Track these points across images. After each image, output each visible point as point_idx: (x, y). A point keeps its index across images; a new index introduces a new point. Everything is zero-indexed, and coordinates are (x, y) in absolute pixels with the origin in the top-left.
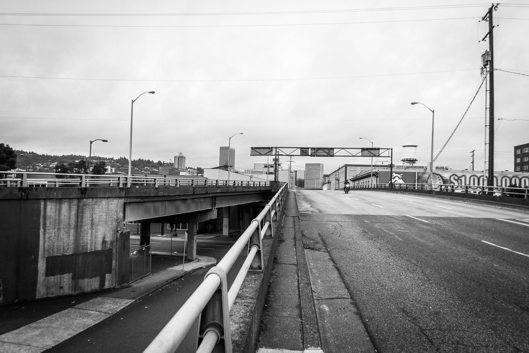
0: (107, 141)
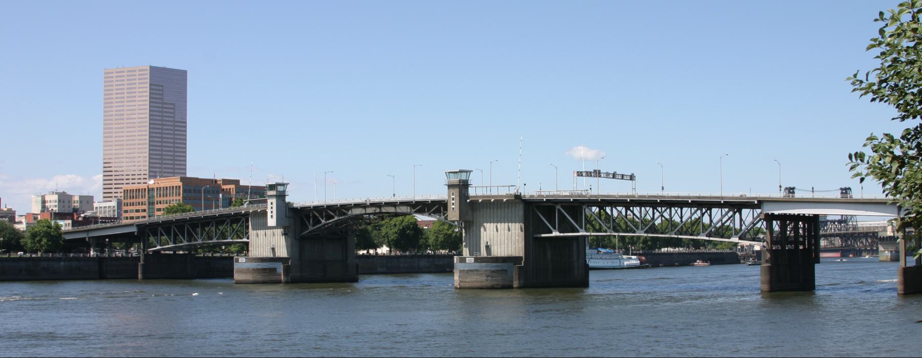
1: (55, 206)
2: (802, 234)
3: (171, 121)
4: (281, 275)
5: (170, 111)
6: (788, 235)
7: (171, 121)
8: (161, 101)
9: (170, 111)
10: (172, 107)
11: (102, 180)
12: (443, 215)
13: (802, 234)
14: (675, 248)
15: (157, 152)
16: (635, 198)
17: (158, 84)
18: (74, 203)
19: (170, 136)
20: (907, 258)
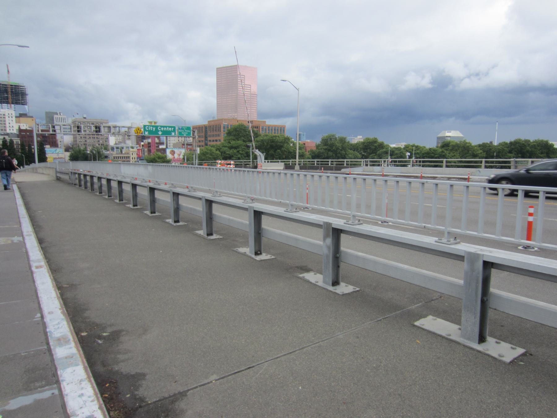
3: (249, 94)
5: (248, 88)
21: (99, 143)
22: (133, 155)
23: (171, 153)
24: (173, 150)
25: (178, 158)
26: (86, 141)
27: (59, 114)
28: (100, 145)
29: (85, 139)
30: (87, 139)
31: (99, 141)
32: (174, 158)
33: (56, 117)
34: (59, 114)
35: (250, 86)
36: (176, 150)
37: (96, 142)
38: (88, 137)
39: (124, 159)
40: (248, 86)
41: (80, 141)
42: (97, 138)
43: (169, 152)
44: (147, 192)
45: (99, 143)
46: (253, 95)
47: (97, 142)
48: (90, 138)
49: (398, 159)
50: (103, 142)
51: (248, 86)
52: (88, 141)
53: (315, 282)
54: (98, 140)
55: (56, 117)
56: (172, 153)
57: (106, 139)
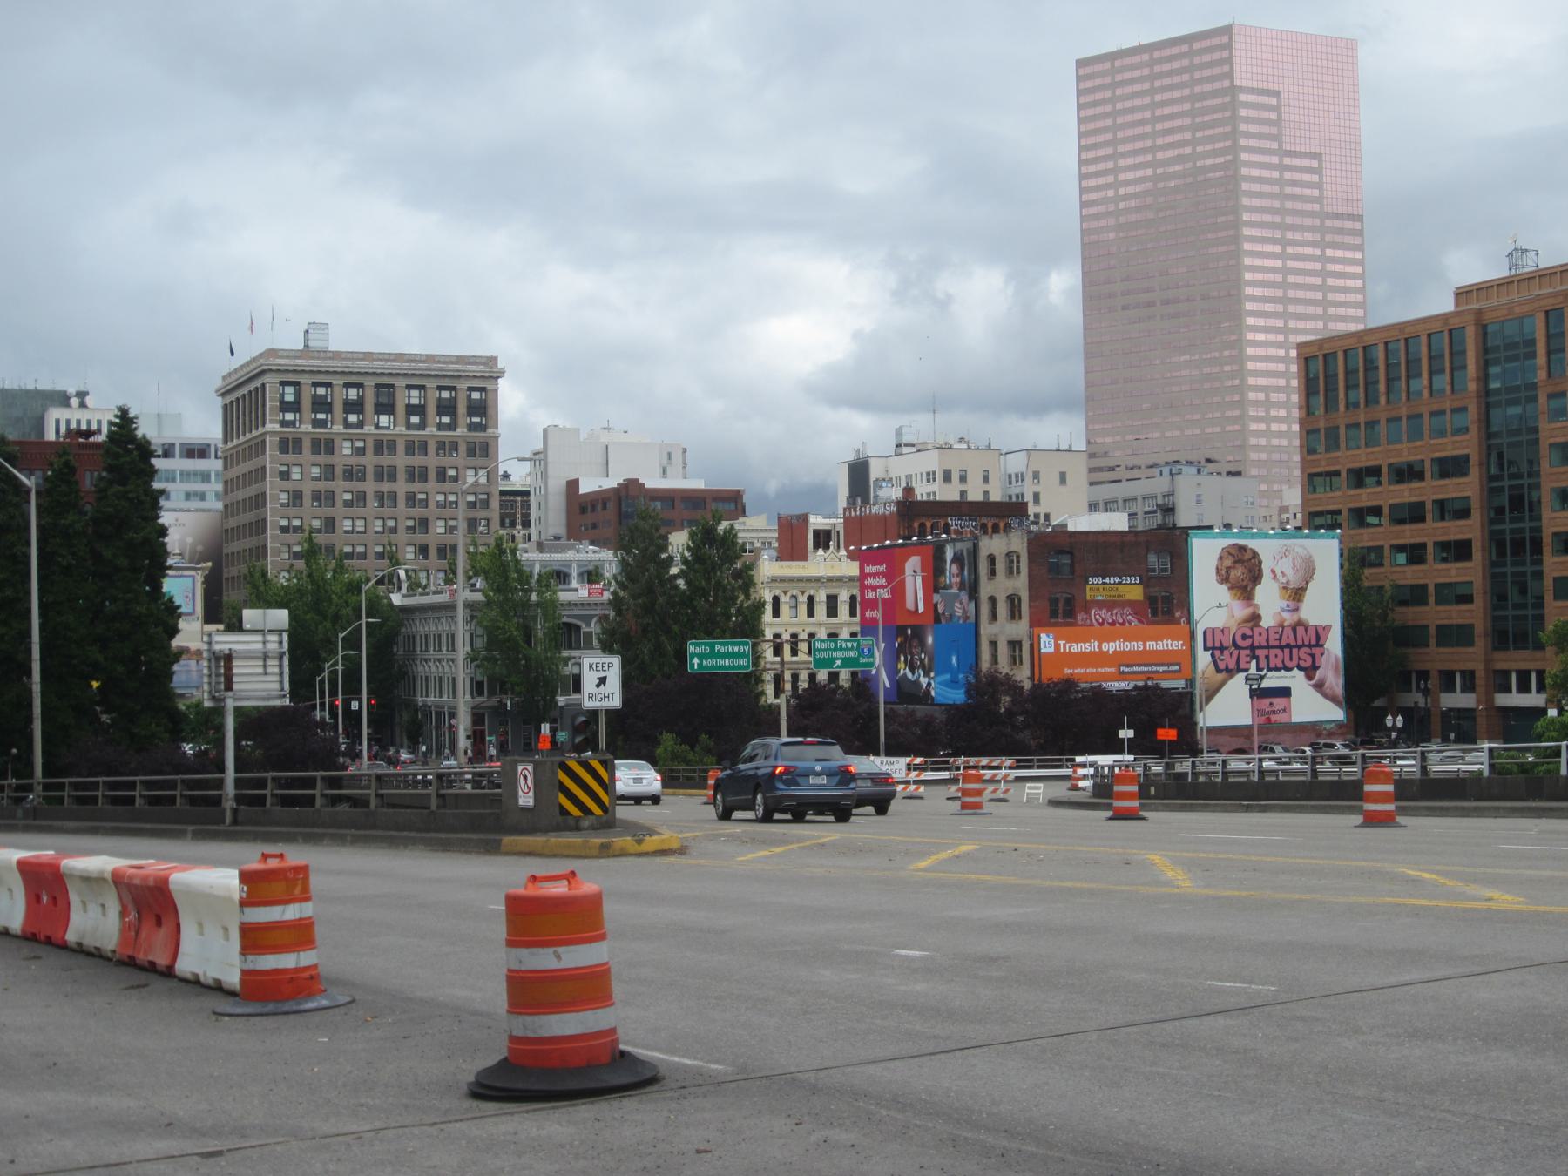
0: (948, 799)
1: (592, 575)
2: (847, 685)
3: (1312, 214)
4: (1512, 582)
5: (1306, 177)
6: (1027, 685)
7: (1312, 214)
8: (1275, 146)
9: (1306, 177)
10: (1315, 164)
11: (1085, 471)
12: (346, 768)
13: (847, 685)
14: (171, 612)
15: (1101, 153)
16: (353, 836)
17: (1265, 86)
18: (1014, 602)
19: (1309, 266)
20: (247, 626)
21: (420, 538)
22: (785, 609)
23: (1224, 577)
24: (1243, 549)
25: (1289, 619)
26: (330, 524)
27: (74, 402)
28: (433, 552)
29: (327, 511)
30: (338, 511)
31: (424, 524)
32: (1255, 618)
33: (58, 422)
34: (74, 402)
35: (1315, 164)
36: (1268, 549)
37: (402, 537)
38: (348, 497)
39: (445, 698)
40: (1306, 163)
41: (284, 523)
42: (411, 498)
43: (1214, 562)
44: (605, 916)
45: (420, 538)
46: (1337, 224)
47: (411, 529)
48: (361, 498)
49: (180, 776)
50: (452, 529)
51: (1306, 163)
52: (347, 525)
53: (227, 938)
54: (418, 512)
55: (58, 422)
56: (1238, 573)
57: (472, 505)
